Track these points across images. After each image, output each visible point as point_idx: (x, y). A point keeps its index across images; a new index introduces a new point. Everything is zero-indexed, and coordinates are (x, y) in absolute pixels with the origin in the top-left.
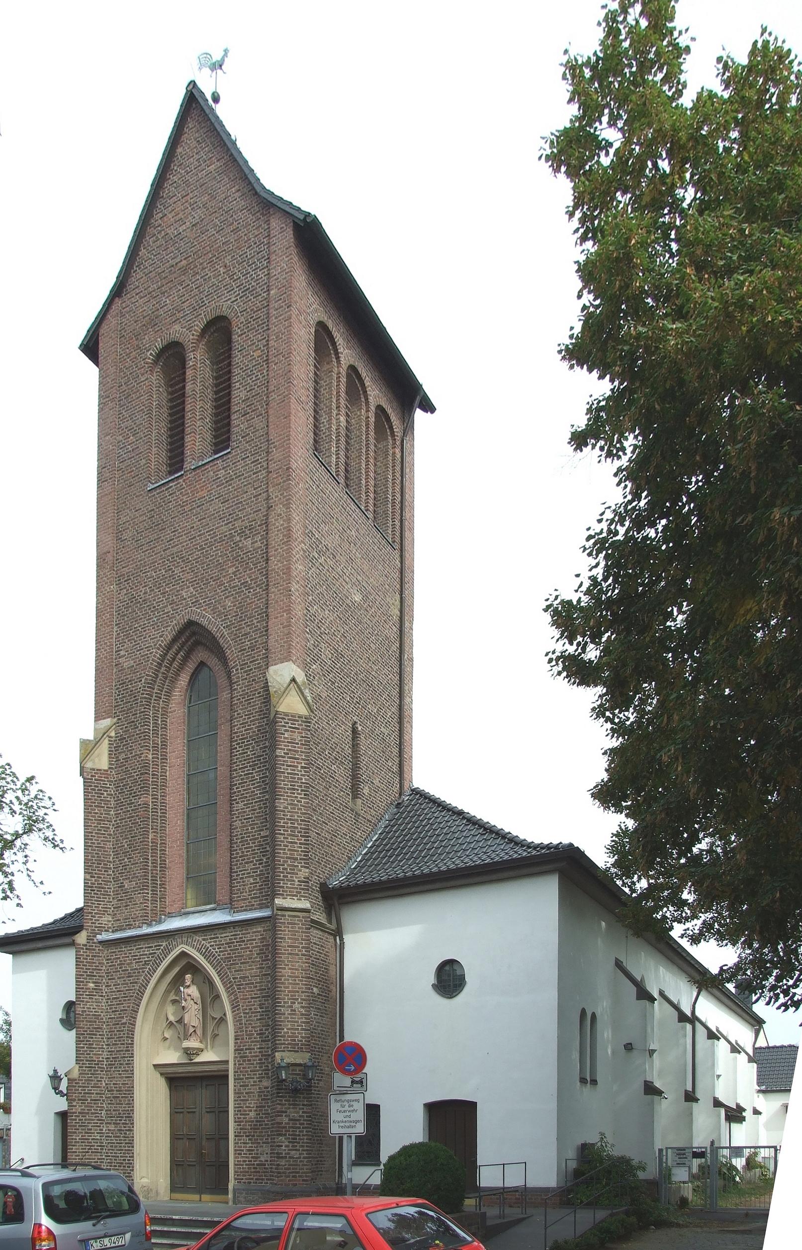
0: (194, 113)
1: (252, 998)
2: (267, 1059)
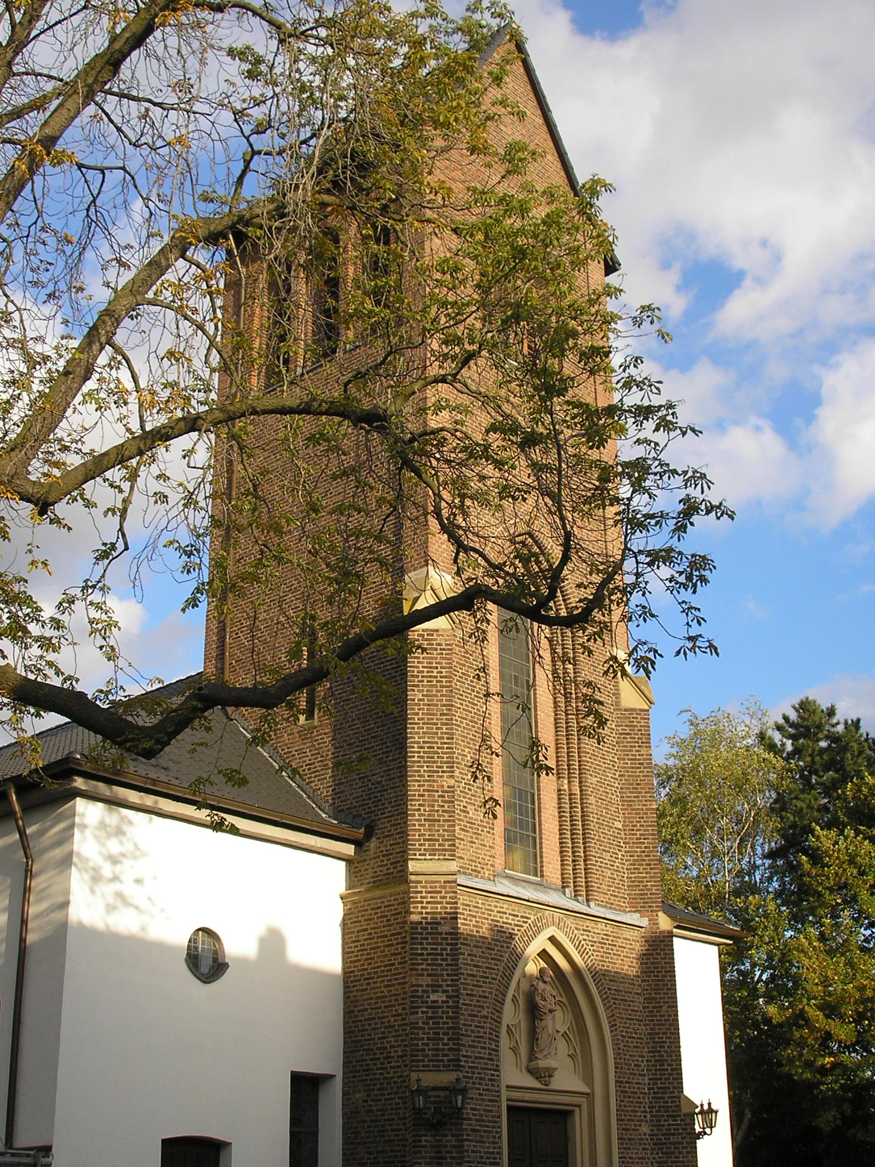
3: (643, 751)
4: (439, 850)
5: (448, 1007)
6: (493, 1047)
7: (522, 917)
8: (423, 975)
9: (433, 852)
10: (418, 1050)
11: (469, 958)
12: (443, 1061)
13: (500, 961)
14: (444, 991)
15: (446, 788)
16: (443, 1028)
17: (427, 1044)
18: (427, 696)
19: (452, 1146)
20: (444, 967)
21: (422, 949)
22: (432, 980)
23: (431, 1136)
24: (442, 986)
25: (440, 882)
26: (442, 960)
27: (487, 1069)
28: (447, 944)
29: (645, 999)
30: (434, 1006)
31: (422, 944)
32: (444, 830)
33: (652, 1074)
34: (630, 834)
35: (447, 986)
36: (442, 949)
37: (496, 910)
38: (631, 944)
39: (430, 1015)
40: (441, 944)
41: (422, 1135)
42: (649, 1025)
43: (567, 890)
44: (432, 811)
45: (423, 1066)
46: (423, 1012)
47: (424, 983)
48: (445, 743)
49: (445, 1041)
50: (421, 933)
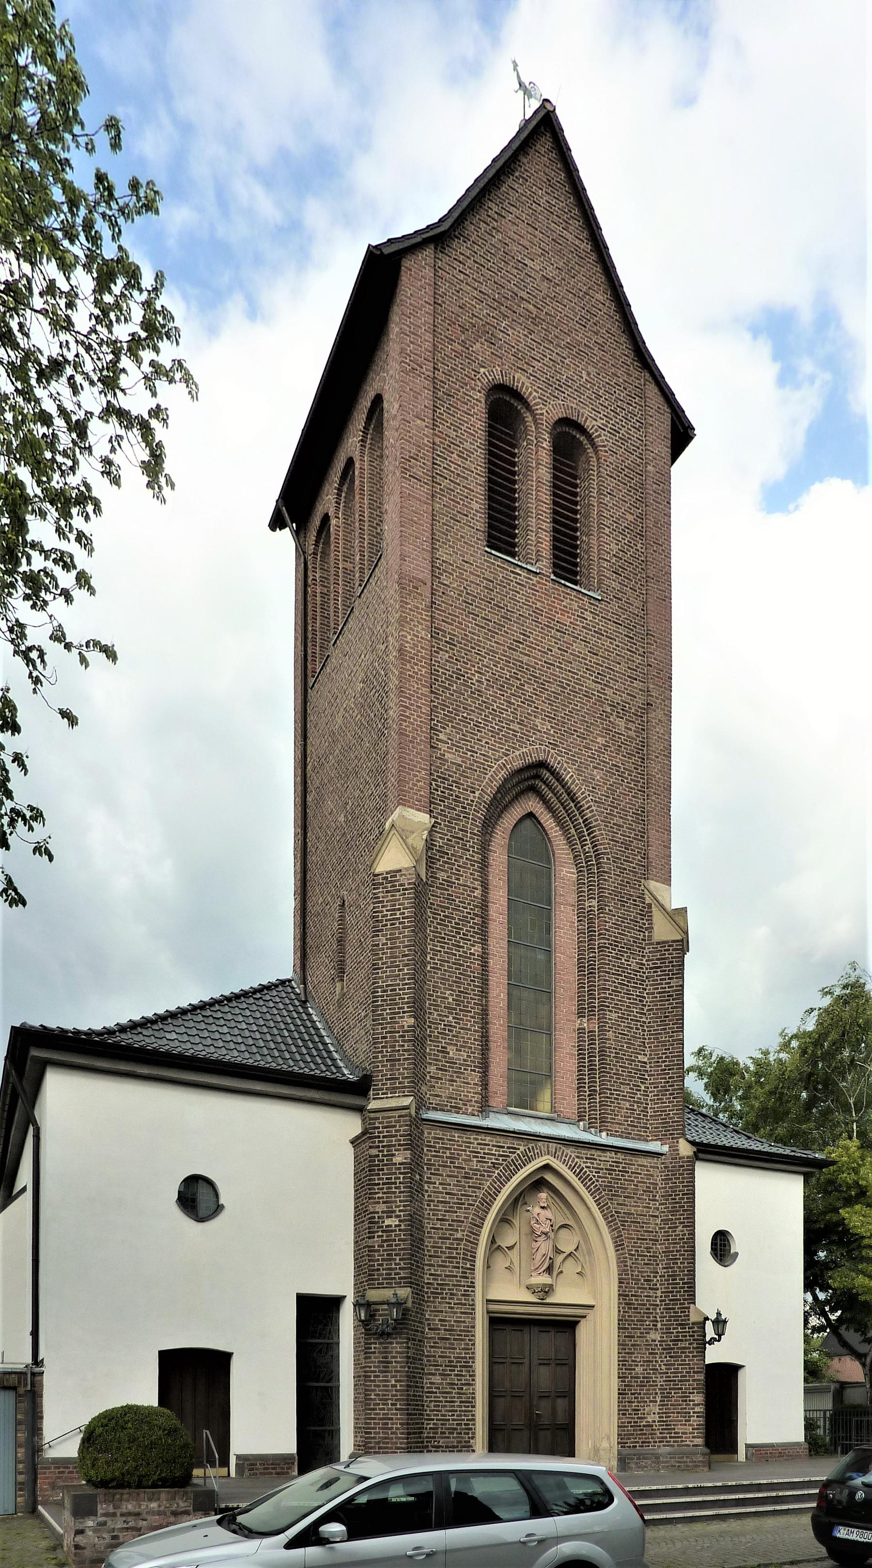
0: (544, 144)
1: (638, 1239)
2: (655, 1309)
3: (673, 983)
4: (399, 1088)
5: (400, 1230)
6: (468, 1266)
7: (508, 1148)
8: (379, 1203)
9: (393, 1090)
10: (373, 1270)
11: (441, 1187)
12: (395, 1278)
13: (479, 1188)
14: (397, 1216)
15: (406, 1028)
16: (395, 1250)
17: (382, 1265)
18: (390, 939)
19: (397, 1352)
20: (398, 1194)
21: (379, 1179)
22: (387, 1207)
23: (380, 1343)
24: (394, 1212)
25: (395, 1117)
26: (396, 1188)
27: (460, 1286)
28: (400, 1173)
29: (662, 1220)
30: (388, 1230)
31: (379, 1175)
32: (404, 1069)
33: (665, 1288)
34: (655, 1066)
35: (400, 1211)
36: (395, 1178)
37: (476, 1142)
38: (647, 1171)
39: (384, 1238)
40: (395, 1173)
41: (371, 1344)
42: (664, 1244)
43: (581, 1123)
44: (393, 1051)
45: (378, 1284)
46: (378, 1236)
47: (380, 1210)
48: (406, 984)
49: (397, 1261)
50: (378, 1165)
